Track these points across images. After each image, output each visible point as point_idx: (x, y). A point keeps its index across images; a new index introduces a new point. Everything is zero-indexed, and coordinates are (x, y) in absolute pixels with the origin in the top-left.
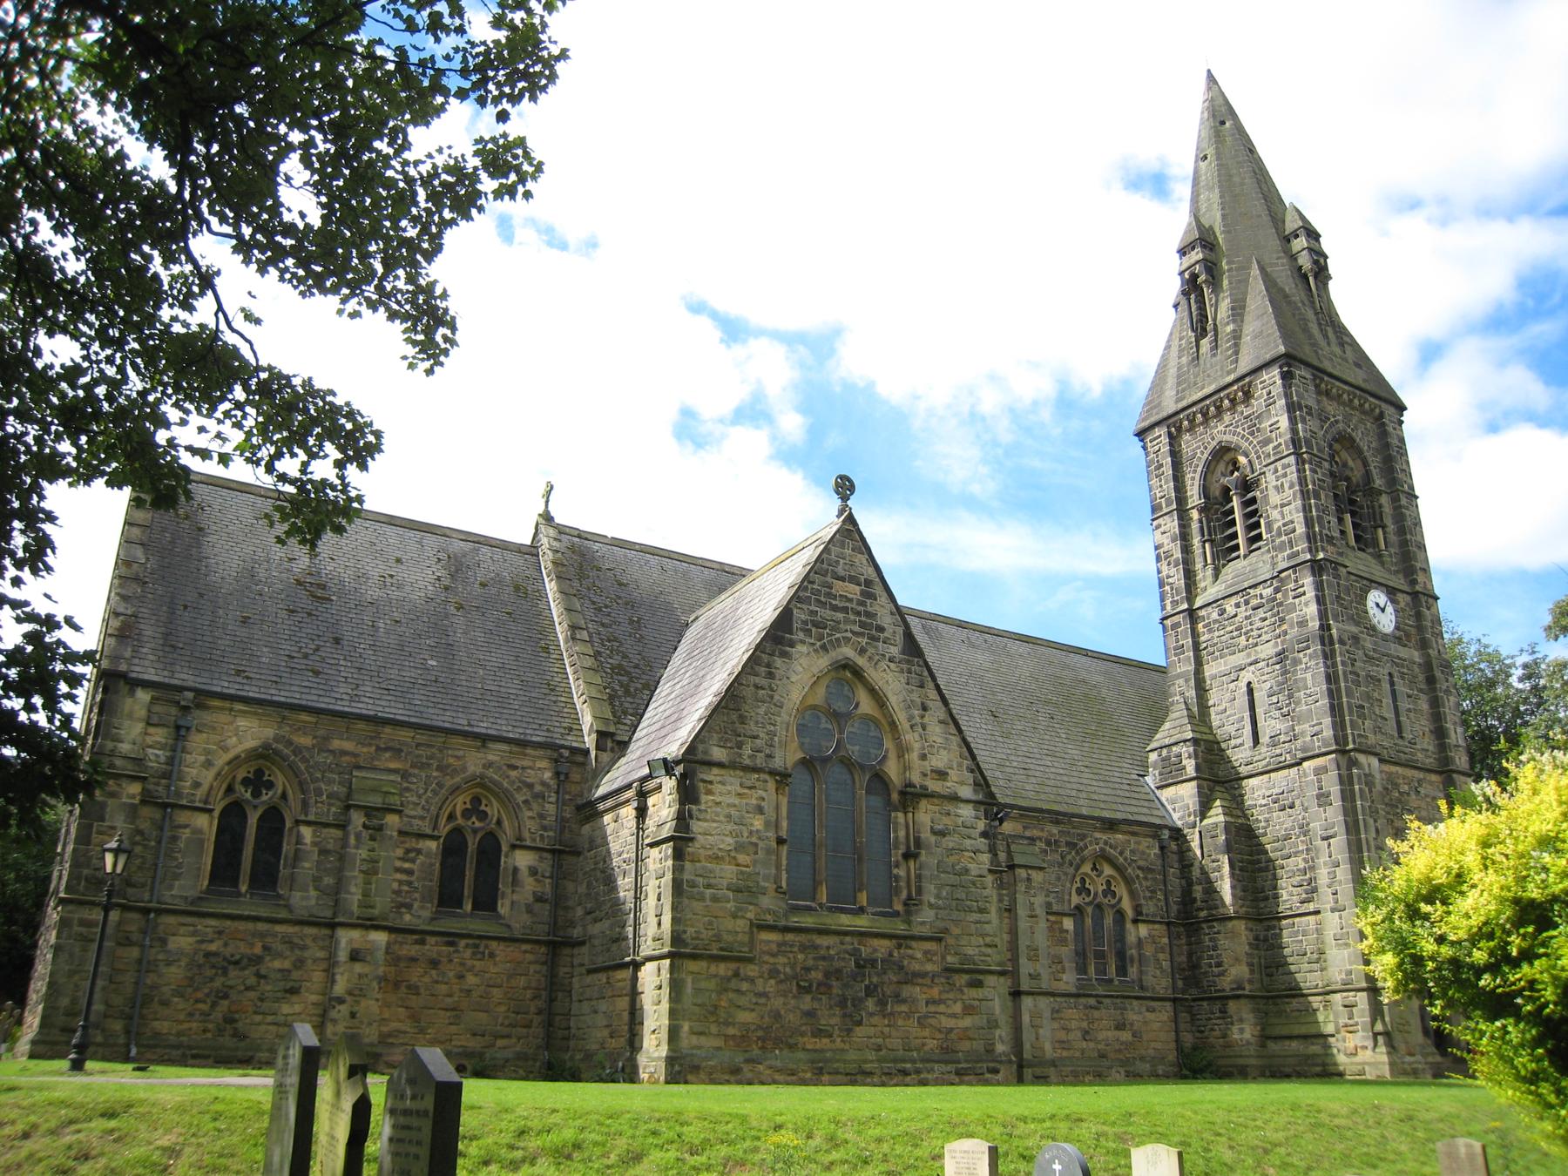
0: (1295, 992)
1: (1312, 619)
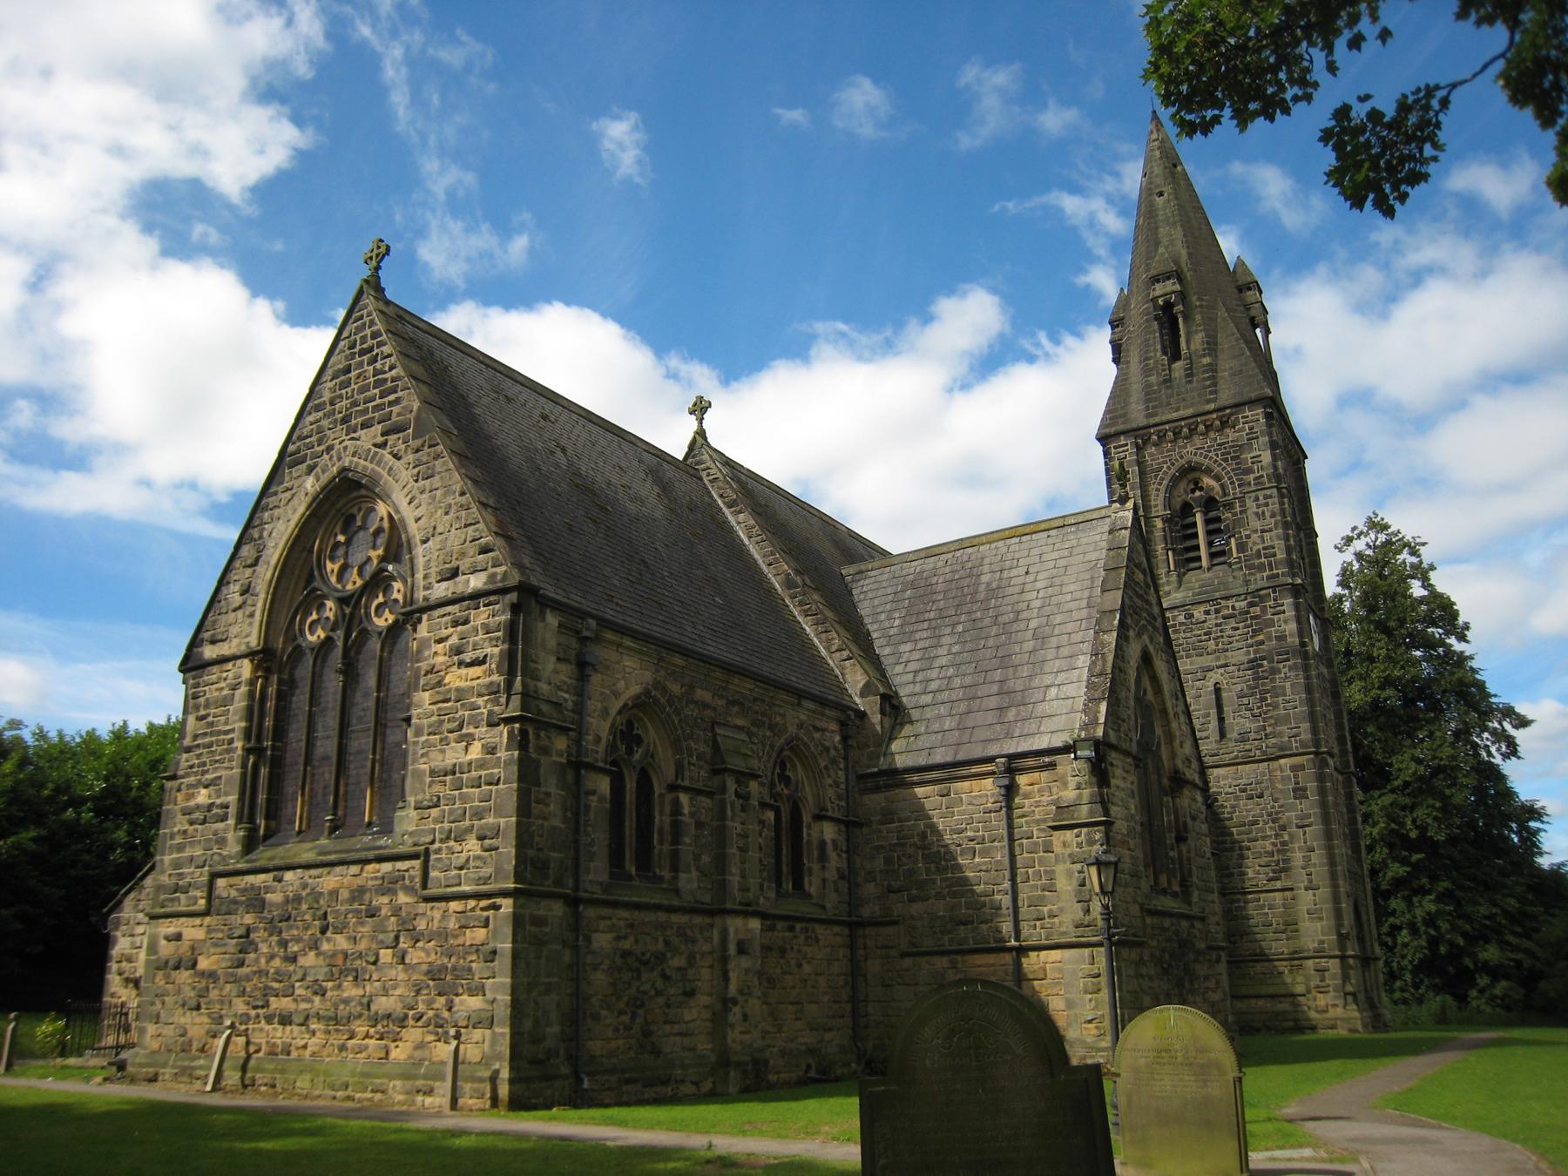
0: (1262, 957)
1: (1292, 635)
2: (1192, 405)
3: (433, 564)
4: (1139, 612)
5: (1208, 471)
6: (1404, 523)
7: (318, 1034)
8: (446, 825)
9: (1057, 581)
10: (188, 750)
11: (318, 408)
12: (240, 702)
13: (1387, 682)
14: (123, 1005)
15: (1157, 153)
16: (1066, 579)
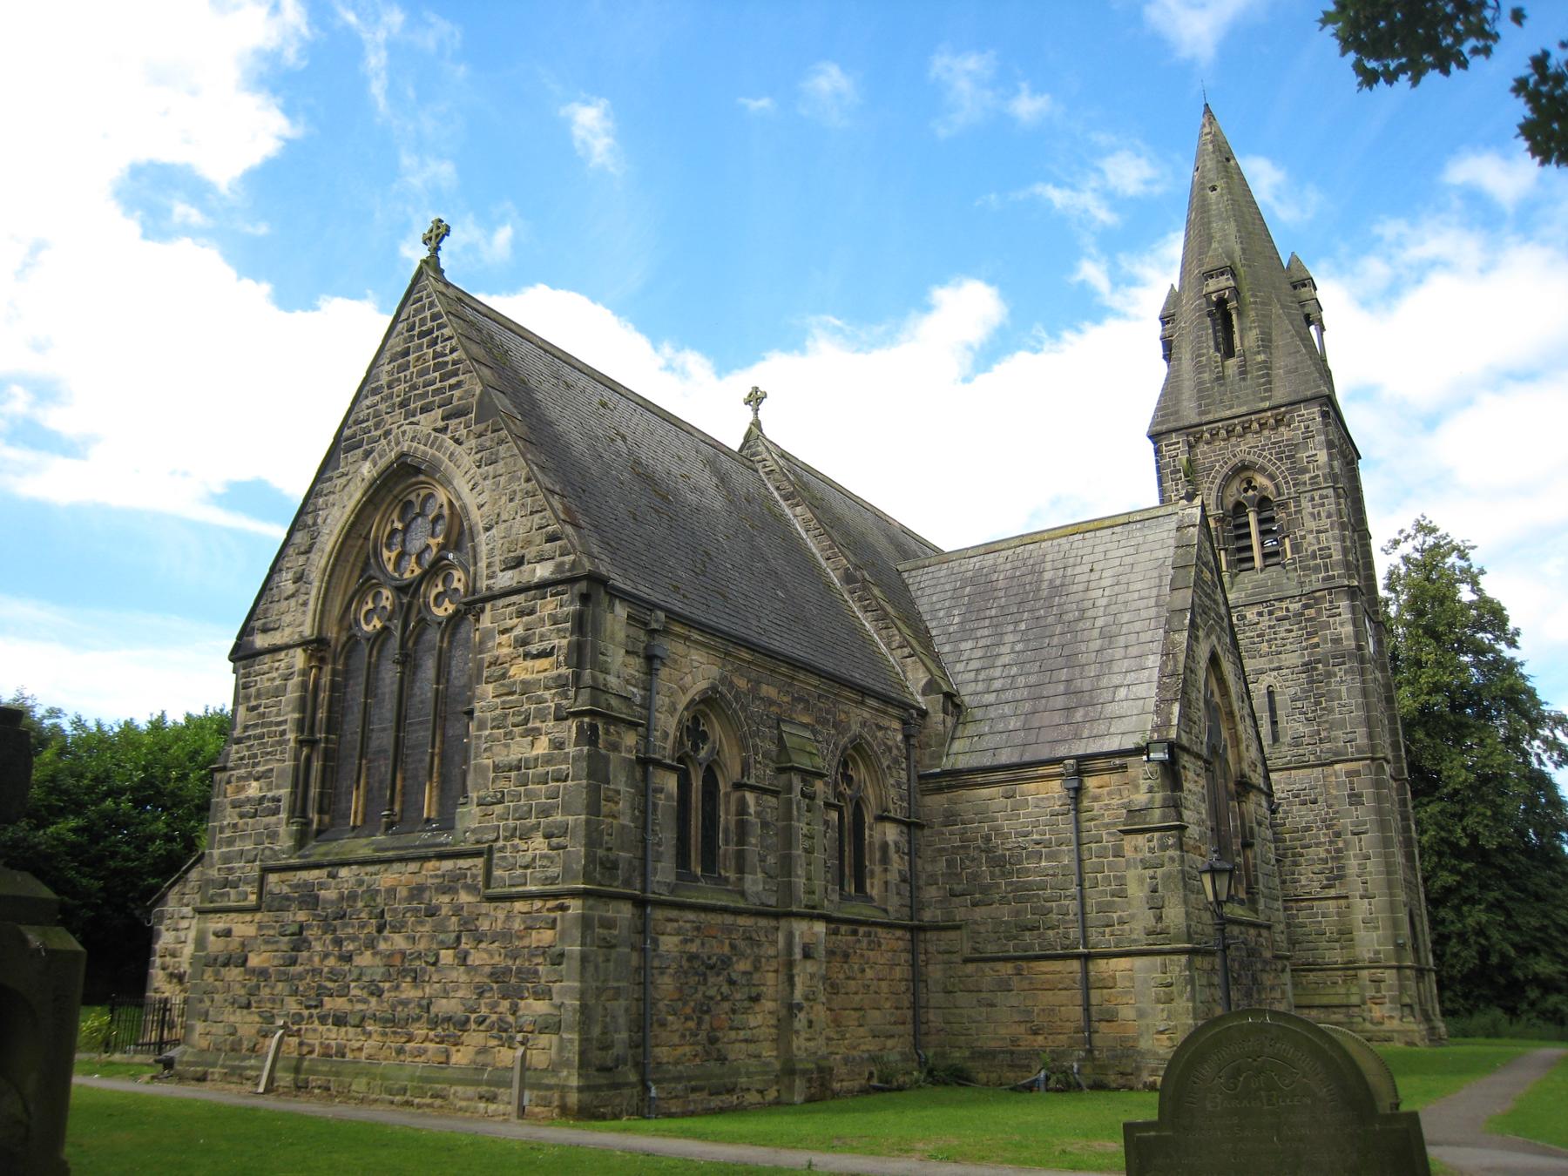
1: (1347, 638)
2: (1245, 403)
3: (496, 552)
4: (1206, 613)
5: (1262, 470)
6: (1453, 528)
7: (375, 1036)
8: (511, 823)
9: (1124, 579)
10: (239, 741)
11: (375, 392)
12: (292, 693)
13: (1436, 688)
14: (166, 1000)
15: (1210, 147)
16: (1133, 577)
